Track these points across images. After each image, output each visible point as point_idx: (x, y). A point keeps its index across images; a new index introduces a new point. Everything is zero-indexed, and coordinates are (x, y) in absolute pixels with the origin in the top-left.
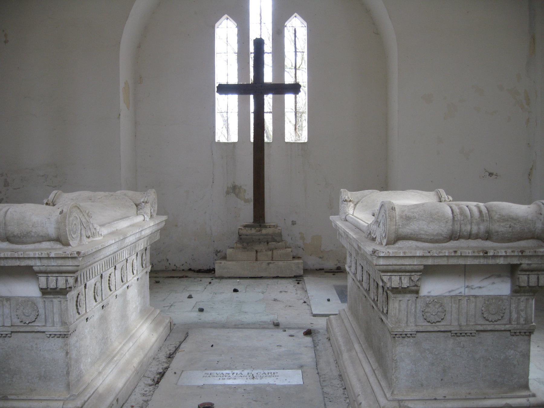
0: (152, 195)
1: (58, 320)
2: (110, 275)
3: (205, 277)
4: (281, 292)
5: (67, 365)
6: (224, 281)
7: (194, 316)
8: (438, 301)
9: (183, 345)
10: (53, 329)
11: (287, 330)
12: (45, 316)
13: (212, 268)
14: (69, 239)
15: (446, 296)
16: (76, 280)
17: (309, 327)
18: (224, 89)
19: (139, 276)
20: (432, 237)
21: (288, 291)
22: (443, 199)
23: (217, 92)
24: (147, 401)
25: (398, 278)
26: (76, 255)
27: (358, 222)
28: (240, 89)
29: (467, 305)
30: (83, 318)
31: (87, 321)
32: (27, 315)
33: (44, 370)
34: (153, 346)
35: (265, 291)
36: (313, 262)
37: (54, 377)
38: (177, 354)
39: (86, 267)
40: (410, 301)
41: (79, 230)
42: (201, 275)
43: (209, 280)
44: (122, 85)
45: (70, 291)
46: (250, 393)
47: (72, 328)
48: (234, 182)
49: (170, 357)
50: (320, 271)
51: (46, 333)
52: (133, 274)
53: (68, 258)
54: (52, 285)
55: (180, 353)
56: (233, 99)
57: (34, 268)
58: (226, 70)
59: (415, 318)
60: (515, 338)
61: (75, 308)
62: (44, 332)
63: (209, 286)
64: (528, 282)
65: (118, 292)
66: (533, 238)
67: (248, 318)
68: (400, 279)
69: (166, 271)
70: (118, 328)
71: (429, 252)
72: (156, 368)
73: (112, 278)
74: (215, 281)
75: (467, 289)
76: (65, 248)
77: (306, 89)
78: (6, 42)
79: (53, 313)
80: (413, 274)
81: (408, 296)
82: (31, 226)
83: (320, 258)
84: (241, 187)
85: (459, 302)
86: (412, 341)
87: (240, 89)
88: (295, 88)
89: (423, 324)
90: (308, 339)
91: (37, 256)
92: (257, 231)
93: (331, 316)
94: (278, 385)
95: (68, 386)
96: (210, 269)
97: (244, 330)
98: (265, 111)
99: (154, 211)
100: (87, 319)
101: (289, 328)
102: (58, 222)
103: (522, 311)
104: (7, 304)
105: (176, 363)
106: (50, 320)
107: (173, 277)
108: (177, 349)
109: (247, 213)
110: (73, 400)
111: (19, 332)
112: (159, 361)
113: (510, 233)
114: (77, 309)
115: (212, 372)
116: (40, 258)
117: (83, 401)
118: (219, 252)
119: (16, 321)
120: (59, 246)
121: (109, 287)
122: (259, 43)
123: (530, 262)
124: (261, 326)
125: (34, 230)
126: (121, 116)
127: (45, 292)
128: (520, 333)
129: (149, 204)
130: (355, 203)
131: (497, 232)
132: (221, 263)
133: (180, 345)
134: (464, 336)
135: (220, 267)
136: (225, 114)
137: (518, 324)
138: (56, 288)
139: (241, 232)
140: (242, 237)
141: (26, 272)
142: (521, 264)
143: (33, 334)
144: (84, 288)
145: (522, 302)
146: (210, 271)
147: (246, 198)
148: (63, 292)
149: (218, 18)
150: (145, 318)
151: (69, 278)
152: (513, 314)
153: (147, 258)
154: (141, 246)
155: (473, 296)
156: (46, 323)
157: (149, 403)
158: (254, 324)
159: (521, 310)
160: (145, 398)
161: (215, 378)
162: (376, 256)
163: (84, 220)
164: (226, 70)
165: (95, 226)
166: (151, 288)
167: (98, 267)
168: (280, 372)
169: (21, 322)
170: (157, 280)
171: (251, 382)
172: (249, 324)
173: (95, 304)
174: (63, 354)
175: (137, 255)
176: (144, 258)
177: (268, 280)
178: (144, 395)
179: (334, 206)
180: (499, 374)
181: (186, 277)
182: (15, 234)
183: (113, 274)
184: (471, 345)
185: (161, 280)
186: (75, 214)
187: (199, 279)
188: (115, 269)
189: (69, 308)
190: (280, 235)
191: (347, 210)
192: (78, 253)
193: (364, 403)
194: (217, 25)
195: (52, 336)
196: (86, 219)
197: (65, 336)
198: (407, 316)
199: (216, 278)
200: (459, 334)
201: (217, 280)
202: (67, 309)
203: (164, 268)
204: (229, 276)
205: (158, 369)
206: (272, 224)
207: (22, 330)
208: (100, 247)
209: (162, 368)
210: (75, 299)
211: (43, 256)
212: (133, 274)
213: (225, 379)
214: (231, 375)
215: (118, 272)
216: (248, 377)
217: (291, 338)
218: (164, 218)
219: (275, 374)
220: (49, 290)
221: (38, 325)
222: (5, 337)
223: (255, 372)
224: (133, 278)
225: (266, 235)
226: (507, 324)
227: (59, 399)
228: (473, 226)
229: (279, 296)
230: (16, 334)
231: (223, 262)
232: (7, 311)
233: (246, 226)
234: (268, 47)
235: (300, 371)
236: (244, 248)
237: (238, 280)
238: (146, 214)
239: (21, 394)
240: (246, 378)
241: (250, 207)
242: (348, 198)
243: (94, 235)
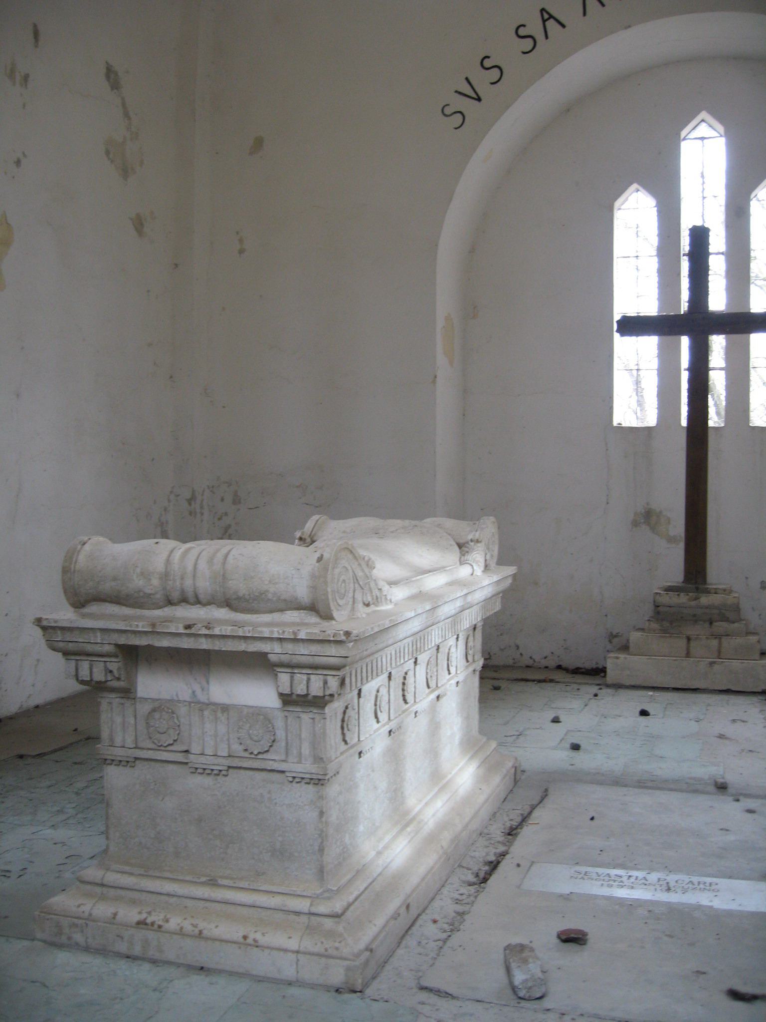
0: (488, 528)
1: (307, 752)
2: (406, 673)
3: (585, 684)
4: (734, 721)
5: (320, 835)
6: (622, 692)
7: (561, 758)
9: (536, 813)
10: (299, 768)
11: (741, 798)
12: (287, 743)
13: (601, 667)
14: (332, 607)
16: (342, 683)
18: (633, 326)
19: (461, 678)
23: (617, 331)
24: (461, 914)
26: (344, 638)
28: (663, 326)
30: (351, 751)
31: (360, 757)
32: (255, 738)
33: (280, 839)
34: (479, 810)
35: (702, 717)
37: (296, 854)
38: (525, 828)
39: (361, 659)
41: (351, 591)
42: (579, 679)
43: (595, 689)
44: (440, 323)
45: (331, 701)
46: (659, 919)
47: (332, 768)
48: (648, 504)
49: (512, 833)
51: (288, 774)
52: (449, 674)
53: (329, 641)
54: (300, 689)
55: (530, 827)
56: (649, 344)
57: (270, 656)
58: (636, 286)
61: (339, 731)
62: (283, 772)
63: (593, 701)
65: (419, 707)
67: (665, 769)
69: (514, 667)
70: (415, 772)
72: (483, 852)
73: (410, 680)
74: (605, 691)
76: (325, 624)
78: (241, 252)
79: (300, 739)
82: (267, 582)
84: (661, 512)
87: (663, 326)
91: (276, 635)
94: (717, 910)
95: (321, 873)
96: (597, 668)
97: (658, 792)
98: (711, 365)
99: (492, 556)
100: (360, 753)
101: (747, 796)
102: (313, 576)
104: (223, 717)
105: (521, 848)
106: (295, 752)
107: (527, 680)
108: (525, 819)
109: (672, 563)
110: (329, 898)
111: (240, 768)
112: (490, 839)
114: (343, 734)
115: (589, 869)
116: (280, 640)
117: (345, 904)
118: (616, 636)
119: (237, 749)
120: (313, 619)
121: (404, 696)
122: (700, 236)
124: (690, 787)
125: (272, 590)
126: (438, 379)
127: (288, 700)
129: (483, 544)
132: (617, 658)
133: (530, 813)
135: (616, 664)
136: (635, 372)
138: (307, 695)
139: (660, 600)
141: (257, 663)
143: (264, 774)
144: (356, 697)
146: (597, 672)
148: (319, 703)
150: (469, 756)
151: (329, 678)
153: (477, 643)
154: (466, 624)
156: (287, 754)
157: (466, 917)
158: (676, 781)
160: (460, 908)
161: (594, 882)
163: (360, 574)
164: (636, 286)
165: (382, 584)
166: (483, 699)
167: (385, 658)
168: (723, 883)
169: (246, 750)
170: (496, 683)
171: (663, 897)
172: (666, 781)
173: (376, 726)
174: (315, 814)
175: (457, 638)
176: (471, 644)
177: (710, 696)
178: (457, 901)
181: (551, 681)
182: (241, 594)
183: (411, 673)
185: (503, 684)
186: (344, 563)
187: (576, 686)
188: (415, 662)
189: (328, 731)
190: (737, 608)
192: (347, 634)
194: (617, 204)
195: (297, 780)
196: (363, 571)
197: (319, 782)
199: (608, 686)
201: (609, 691)
202: (324, 733)
203: (511, 662)
204: (633, 684)
205: (487, 854)
206: (721, 587)
207: (245, 765)
208: (387, 624)
209: (495, 854)
210: (340, 717)
211: (286, 636)
212: (449, 674)
213: (612, 886)
214: (625, 879)
215: (421, 671)
216: (658, 887)
217: (749, 815)
218: (511, 570)
219: (713, 887)
220: (294, 697)
221: (274, 759)
222: (218, 775)
223: (672, 878)
224: (449, 680)
227: (305, 894)
229: (730, 730)
230: (236, 771)
231: (622, 656)
232: (222, 729)
233: (669, 589)
234: (717, 242)
236: (664, 631)
237: (651, 693)
238: (477, 562)
239: (241, 879)
240: (652, 888)
243: (377, 601)
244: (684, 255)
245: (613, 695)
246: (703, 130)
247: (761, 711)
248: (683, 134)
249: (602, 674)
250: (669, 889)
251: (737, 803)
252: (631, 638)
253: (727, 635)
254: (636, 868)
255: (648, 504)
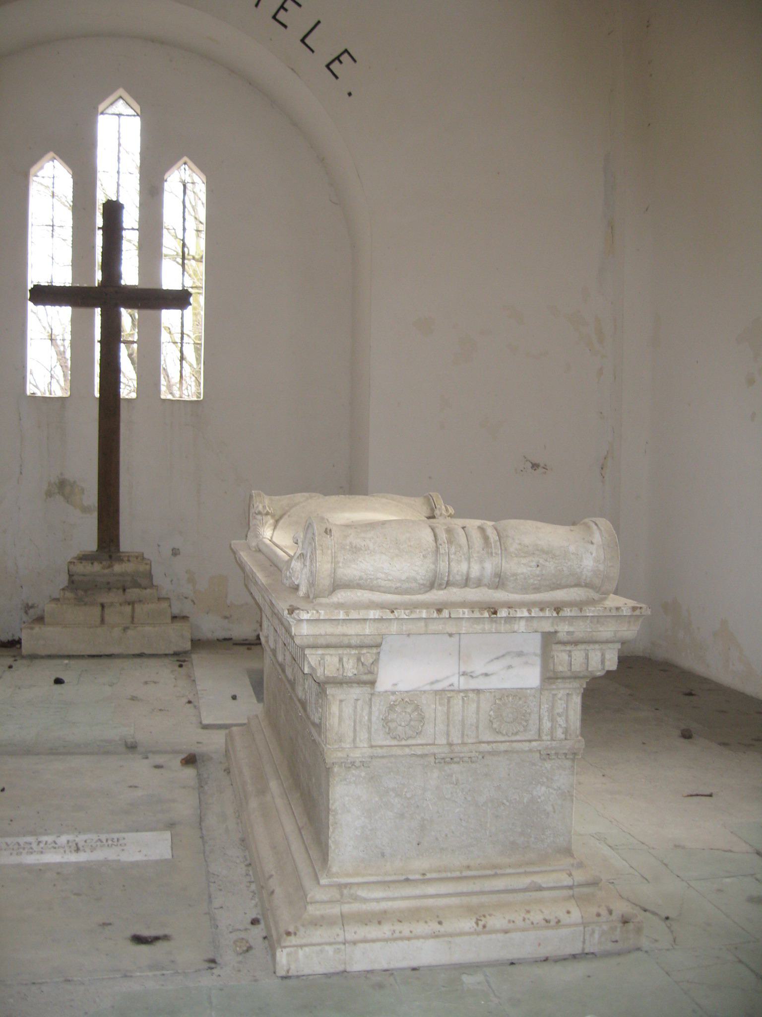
8: (410, 701)
11: (150, 755)
13: (17, 638)
15: (425, 692)
17: (195, 749)
18: (45, 295)
20: (398, 585)
21: (163, 682)
22: (437, 512)
23: (30, 300)
25: (336, 660)
27: (275, 554)
28: (72, 296)
29: (463, 706)
36: (211, 626)
40: (359, 702)
43: (10, 661)
48: (62, 474)
50: (226, 644)
58: (50, 258)
59: (369, 732)
60: (548, 765)
64: (603, 662)
66: (577, 585)
68: (341, 660)
71: (393, 612)
75: (462, 679)
77: (202, 299)
80: (364, 651)
81: (356, 692)
83: (226, 618)
84: (75, 482)
85: (449, 701)
86: (363, 774)
87: (72, 296)
88: (180, 299)
89: (385, 743)
90: (190, 772)
92: (103, 568)
93: (234, 729)
101: (154, 753)
103: (559, 715)
109: (87, 535)
113: (538, 576)
118: (32, 607)
122: (113, 210)
123: (571, 629)
124: (102, 749)
128: (557, 754)
130: (277, 517)
131: (514, 575)
134: (458, 763)
137: (552, 739)
139: (74, 569)
140: (75, 578)
142: (556, 632)
145: (560, 699)
147: (86, 504)
149: (35, 159)
152: (544, 721)
155: (473, 690)
159: (558, 714)
162: (294, 618)
164: (50, 258)
168: (130, 837)
171: (73, 858)
179: (246, 523)
180: (520, 830)
184: (470, 780)
190: (149, 575)
191: (261, 530)
193: (278, 891)
194: (33, 170)
198: (355, 730)
199: (23, 657)
200: (448, 760)
201: (25, 662)
204: (49, 653)
214: (34, 846)
217: (157, 771)
219: (121, 842)
223: (81, 839)
225: (122, 575)
226: (535, 740)
228: (472, 564)
233: (84, 558)
234: (130, 218)
235: (167, 835)
237: (66, 661)
240: (62, 850)
241: (91, 523)
242: (264, 507)
244: (99, 228)
245: (29, 666)
246: (120, 106)
247: (172, 671)
248: (101, 108)
249: (18, 646)
250: (78, 850)
251: (146, 761)
252: (46, 609)
253: (140, 601)
254: (46, 833)
255: (62, 474)
